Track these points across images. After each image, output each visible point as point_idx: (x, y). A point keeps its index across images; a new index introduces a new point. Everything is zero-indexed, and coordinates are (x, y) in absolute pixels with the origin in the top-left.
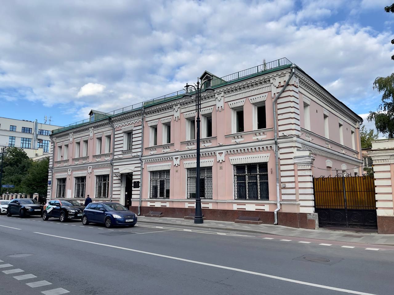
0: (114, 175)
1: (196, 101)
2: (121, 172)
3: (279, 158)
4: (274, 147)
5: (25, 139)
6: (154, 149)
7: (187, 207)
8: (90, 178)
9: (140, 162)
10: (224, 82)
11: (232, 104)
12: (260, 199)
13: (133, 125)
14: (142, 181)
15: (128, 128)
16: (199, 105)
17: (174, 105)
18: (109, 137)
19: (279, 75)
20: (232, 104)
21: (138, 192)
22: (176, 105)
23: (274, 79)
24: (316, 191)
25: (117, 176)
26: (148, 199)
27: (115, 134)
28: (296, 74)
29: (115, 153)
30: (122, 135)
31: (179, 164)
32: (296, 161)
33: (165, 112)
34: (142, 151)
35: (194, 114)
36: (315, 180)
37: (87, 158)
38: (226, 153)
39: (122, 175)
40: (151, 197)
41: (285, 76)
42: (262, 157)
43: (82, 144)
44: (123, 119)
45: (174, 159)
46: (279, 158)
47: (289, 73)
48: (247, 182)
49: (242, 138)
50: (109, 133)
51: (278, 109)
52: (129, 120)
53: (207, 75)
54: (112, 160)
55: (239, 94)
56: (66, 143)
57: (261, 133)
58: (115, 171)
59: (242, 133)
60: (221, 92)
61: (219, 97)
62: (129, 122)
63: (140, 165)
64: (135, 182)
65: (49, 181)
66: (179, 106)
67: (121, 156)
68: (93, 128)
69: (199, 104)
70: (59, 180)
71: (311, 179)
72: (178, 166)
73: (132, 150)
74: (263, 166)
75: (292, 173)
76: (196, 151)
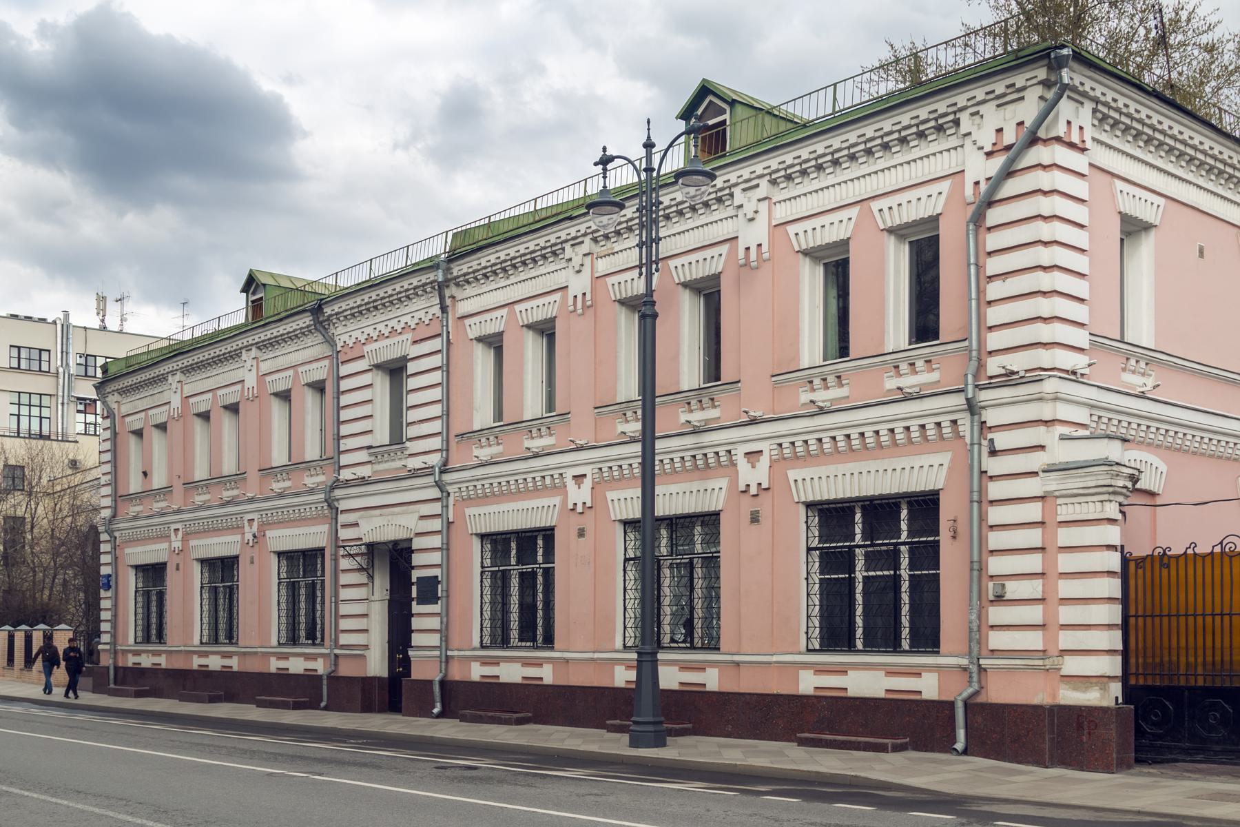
2: (366, 540)
4: (965, 421)
5: (25, 399)
6: (492, 438)
8: (178, 569)
9: (435, 493)
10: (790, 125)
12: (817, 647)
13: (409, 336)
15: (388, 350)
16: (649, 243)
17: (566, 241)
19: (998, 97)
21: (435, 623)
22: (576, 242)
23: (977, 113)
26: (474, 649)
27: (341, 375)
28: (1074, 89)
32: (1052, 483)
33: (533, 273)
36: (1132, 566)
37: (240, 479)
39: (372, 549)
40: (487, 640)
41: (1023, 98)
42: (687, 493)
44: (376, 308)
45: (571, 484)
46: (986, 472)
47: (1039, 83)
48: (859, 576)
49: (715, 407)
50: (319, 372)
51: (990, 254)
52: (407, 310)
53: (710, 98)
54: (332, 488)
55: (833, 186)
56: (160, 416)
57: (920, 364)
58: (344, 534)
59: (844, 366)
60: (979, 103)
61: (749, 201)
62: (393, 323)
63: (436, 508)
65: (104, 576)
66: (587, 245)
67: (365, 471)
68: (254, 348)
69: (652, 241)
70: (497, 542)
71: (1113, 561)
72: (763, 494)
73: (408, 444)
76: (637, 448)
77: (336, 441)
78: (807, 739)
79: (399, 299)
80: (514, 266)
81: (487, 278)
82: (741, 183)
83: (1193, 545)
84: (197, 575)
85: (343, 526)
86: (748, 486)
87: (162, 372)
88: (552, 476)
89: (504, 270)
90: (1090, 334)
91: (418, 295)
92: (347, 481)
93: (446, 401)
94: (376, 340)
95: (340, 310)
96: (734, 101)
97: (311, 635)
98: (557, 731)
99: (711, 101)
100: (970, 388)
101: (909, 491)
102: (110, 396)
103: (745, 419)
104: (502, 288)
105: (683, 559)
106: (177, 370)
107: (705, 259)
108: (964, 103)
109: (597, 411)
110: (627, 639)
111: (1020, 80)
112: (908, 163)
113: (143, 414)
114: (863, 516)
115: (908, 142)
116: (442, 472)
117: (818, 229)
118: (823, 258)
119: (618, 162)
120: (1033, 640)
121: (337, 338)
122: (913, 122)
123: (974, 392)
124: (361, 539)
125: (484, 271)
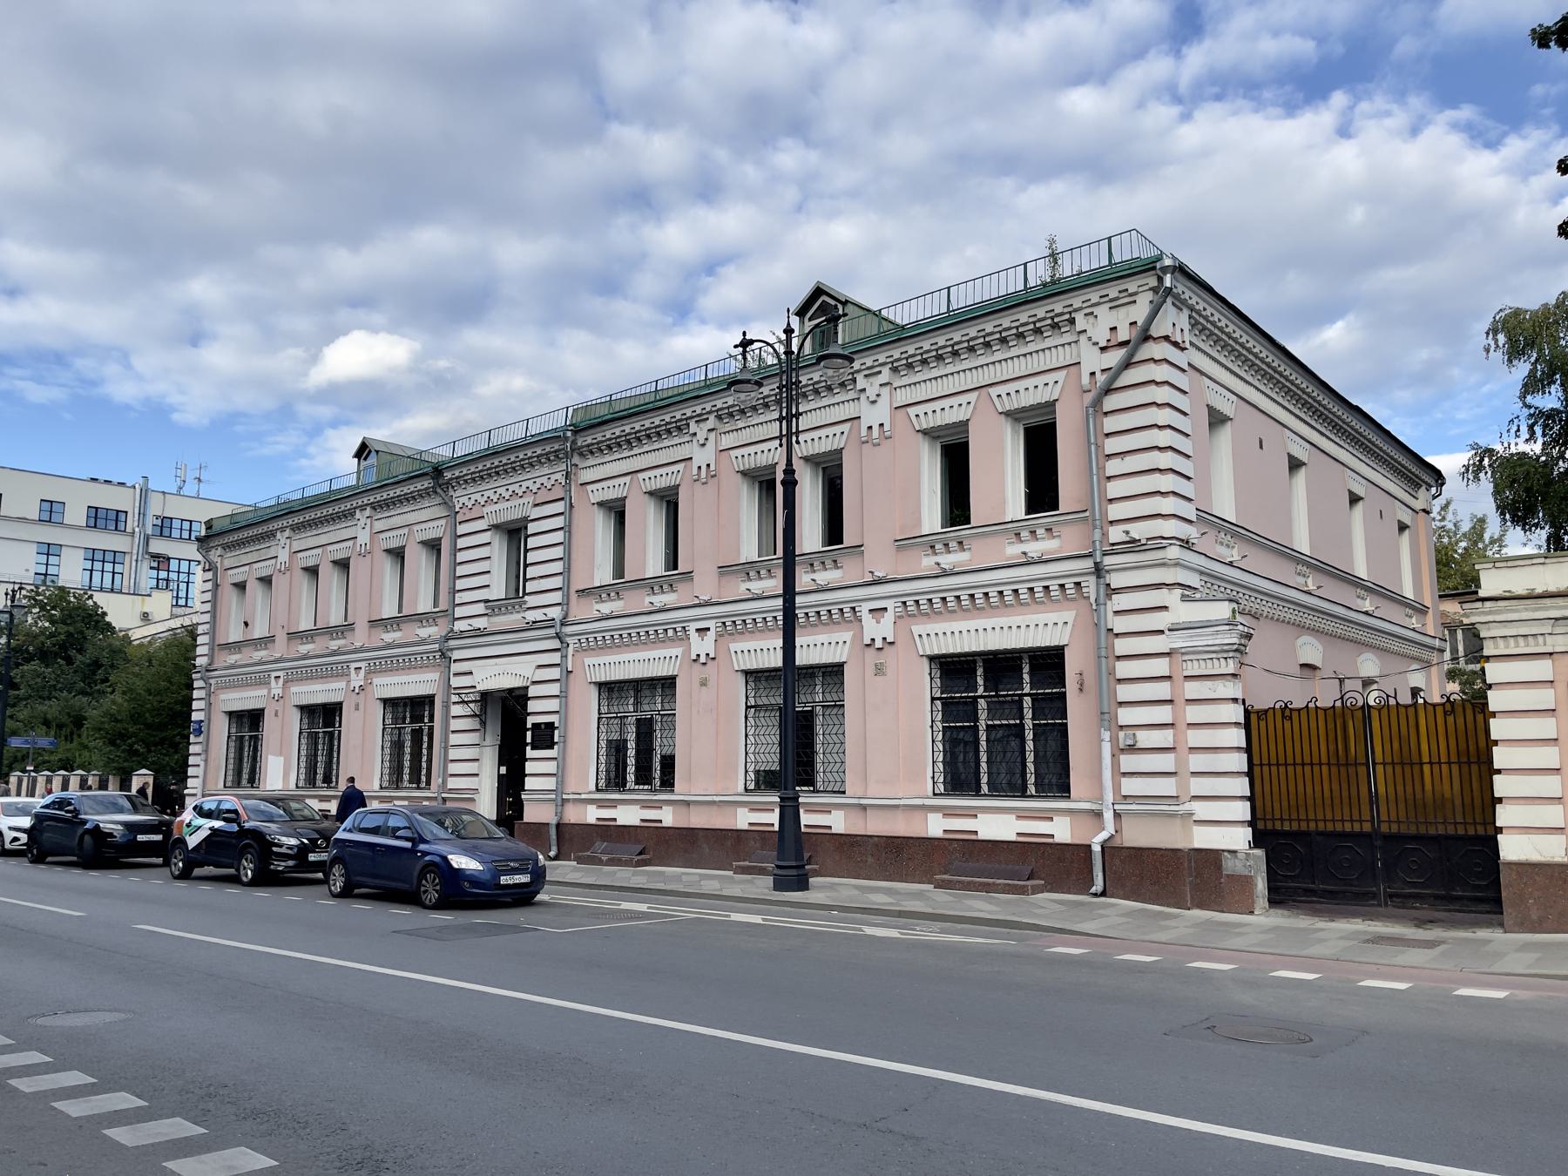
0: (455, 698)
1: (779, 402)
2: (480, 687)
3: (1112, 630)
4: (1090, 584)
5: (99, 556)
7: (746, 827)
8: (276, 715)
9: (555, 644)
10: (891, 327)
11: (922, 416)
12: (1034, 793)
13: (530, 499)
14: (565, 720)
15: (509, 512)
16: (790, 417)
18: (433, 546)
19: (1111, 300)
20: (922, 416)
21: (551, 767)
22: (701, 419)
23: (1092, 313)
24: (1256, 761)
25: (467, 703)
26: (590, 793)
28: (1177, 297)
29: (459, 612)
30: (485, 538)
31: (712, 655)
32: (1178, 641)
34: (565, 604)
35: (772, 455)
36: (1254, 718)
38: (900, 609)
40: (602, 783)
41: (1135, 302)
43: (326, 571)
45: (694, 635)
46: (1112, 630)
47: (1150, 289)
49: (838, 568)
51: (1107, 435)
54: (447, 639)
56: (263, 569)
58: (456, 682)
59: (962, 531)
60: (881, 365)
61: (872, 387)
64: (536, 726)
65: (195, 722)
67: (480, 623)
71: (1236, 712)
72: (710, 662)
74: (1049, 662)
75: (1162, 690)
76: (780, 602)
77: (452, 594)
78: (943, 881)
79: (522, 466)
80: (639, 439)
81: (620, 446)
82: (864, 369)
83: (1314, 699)
84: (294, 720)
85: (455, 675)
86: (873, 640)
87: (271, 529)
88: (675, 629)
89: (629, 442)
90: (1197, 509)
91: (541, 463)
92: (461, 632)
93: (567, 559)
94: (496, 503)
95: (461, 474)
96: (847, 302)
97: (327, 779)
98: (620, 870)
99: (823, 301)
100: (1098, 553)
101: (1052, 645)
102: (214, 550)
103: (869, 578)
104: (625, 458)
105: (806, 706)
106: (287, 527)
107: (770, 450)
108: (1060, 311)
109: (897, 543)
110: (748, 783)
111: (1132, 287)
112: (1025, 355)
113: (247, 568)
114: (985, 671)
115: (1025, 338)
116: (562, 624)
117: (816, 440)
118: (1023, 419)
119: (757, 345)
120: (1166, 787)
121: (455, 501)
122: (1031, 320)
123: (1102, 558)
124: (475, 687)
125: (608, 443)
